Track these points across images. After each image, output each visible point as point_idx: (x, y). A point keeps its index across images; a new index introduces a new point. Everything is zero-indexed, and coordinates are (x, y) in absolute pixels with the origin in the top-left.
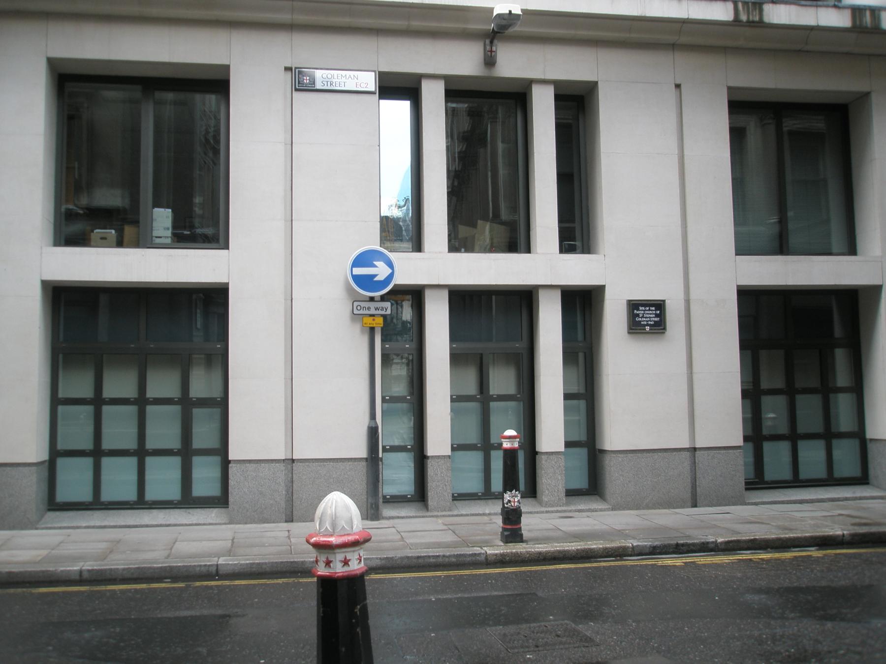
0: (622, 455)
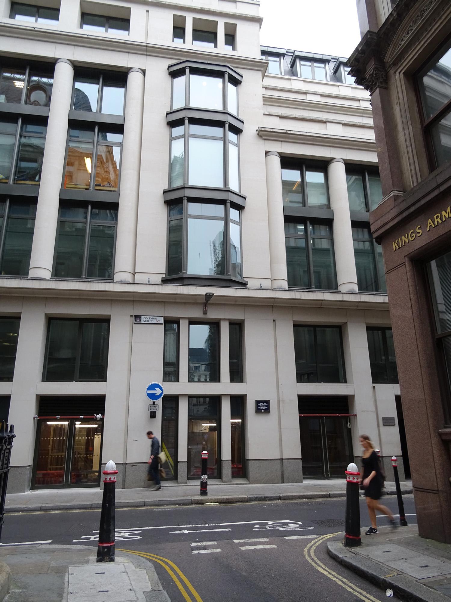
0: (254, 461)
